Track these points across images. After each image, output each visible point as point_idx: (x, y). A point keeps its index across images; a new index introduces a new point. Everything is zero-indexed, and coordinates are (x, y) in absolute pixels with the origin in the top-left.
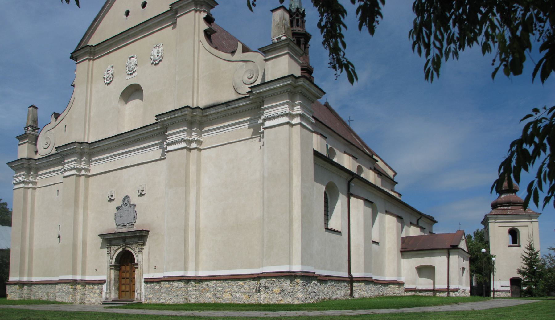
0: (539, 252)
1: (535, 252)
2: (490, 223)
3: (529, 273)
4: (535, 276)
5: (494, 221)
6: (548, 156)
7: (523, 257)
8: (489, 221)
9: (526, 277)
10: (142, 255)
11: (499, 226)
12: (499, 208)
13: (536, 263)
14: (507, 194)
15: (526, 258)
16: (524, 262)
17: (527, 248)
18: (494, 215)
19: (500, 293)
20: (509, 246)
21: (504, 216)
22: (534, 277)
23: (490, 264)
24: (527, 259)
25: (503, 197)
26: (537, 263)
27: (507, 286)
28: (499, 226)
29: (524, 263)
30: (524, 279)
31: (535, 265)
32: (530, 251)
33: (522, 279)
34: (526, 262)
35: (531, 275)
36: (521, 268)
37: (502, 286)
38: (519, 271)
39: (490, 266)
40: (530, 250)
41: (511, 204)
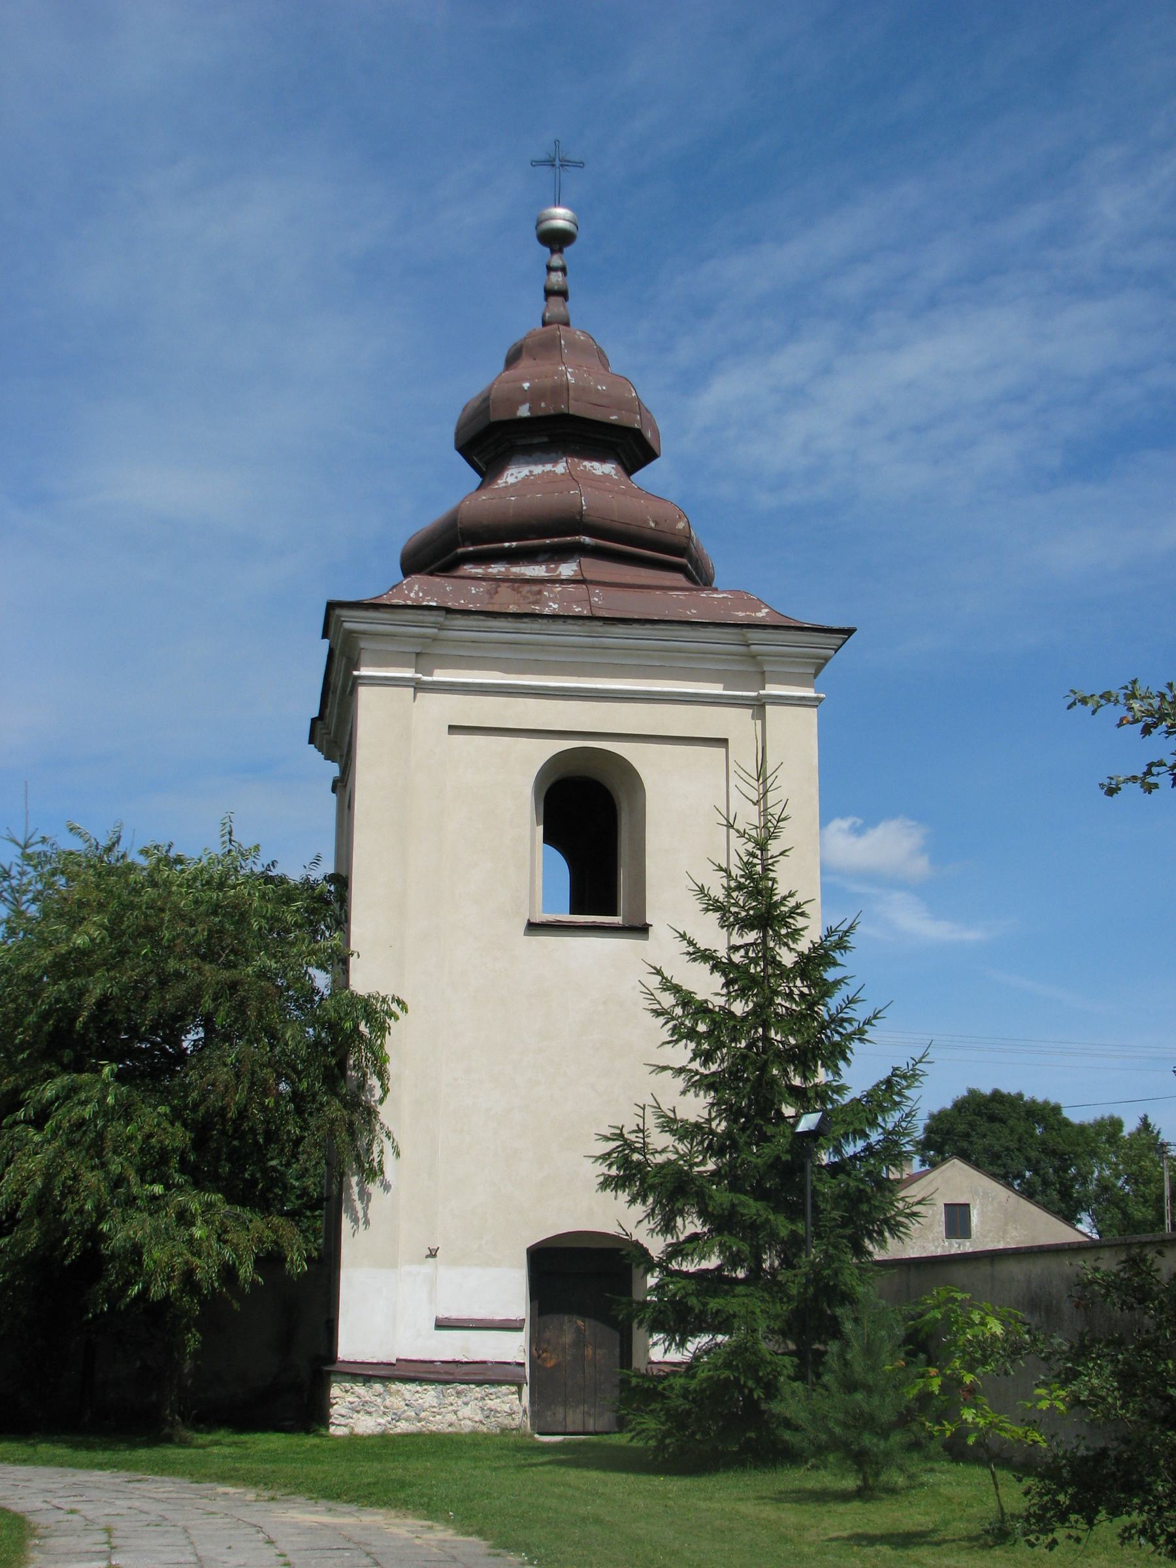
0: (841, 945)
1: (803, 946)
2: (364, 693)
3: (734, 1187)
4: (794, 1212)
5: (409, 673)
6: (777, 1225)
7: (668, 1000)
8: (364, 671)
9: (690, 1225)
10: (230, 1526)
11: (453, 729)
12: (469, 569)
13: (807, 1071)
14: (555, 462)
15: (703, 1010)
16: (682, 1054)
17: (714, 906)
18: (410, 616)
19: (428, 1396)
20: (534, 927)
21: (501, 631)
22: (784, 1227)
23: (333, 1091)
24: (721, 1021)
25: (511, 480)
26: (822, 1076)
27: (500, 1315)
28: (453, 729)
29: (681, 1071)
30: (676, 1251)
31: (799, 1096)
32: (752, 936)
33: (644, 1252)
34: (708, 1057)
35: (752, 1208)
36: (651, 1122)
37: (442, 1325)
38: (625, 1163)
39: (335, 1110)
40: (746, 924)
41: (587, 540)
